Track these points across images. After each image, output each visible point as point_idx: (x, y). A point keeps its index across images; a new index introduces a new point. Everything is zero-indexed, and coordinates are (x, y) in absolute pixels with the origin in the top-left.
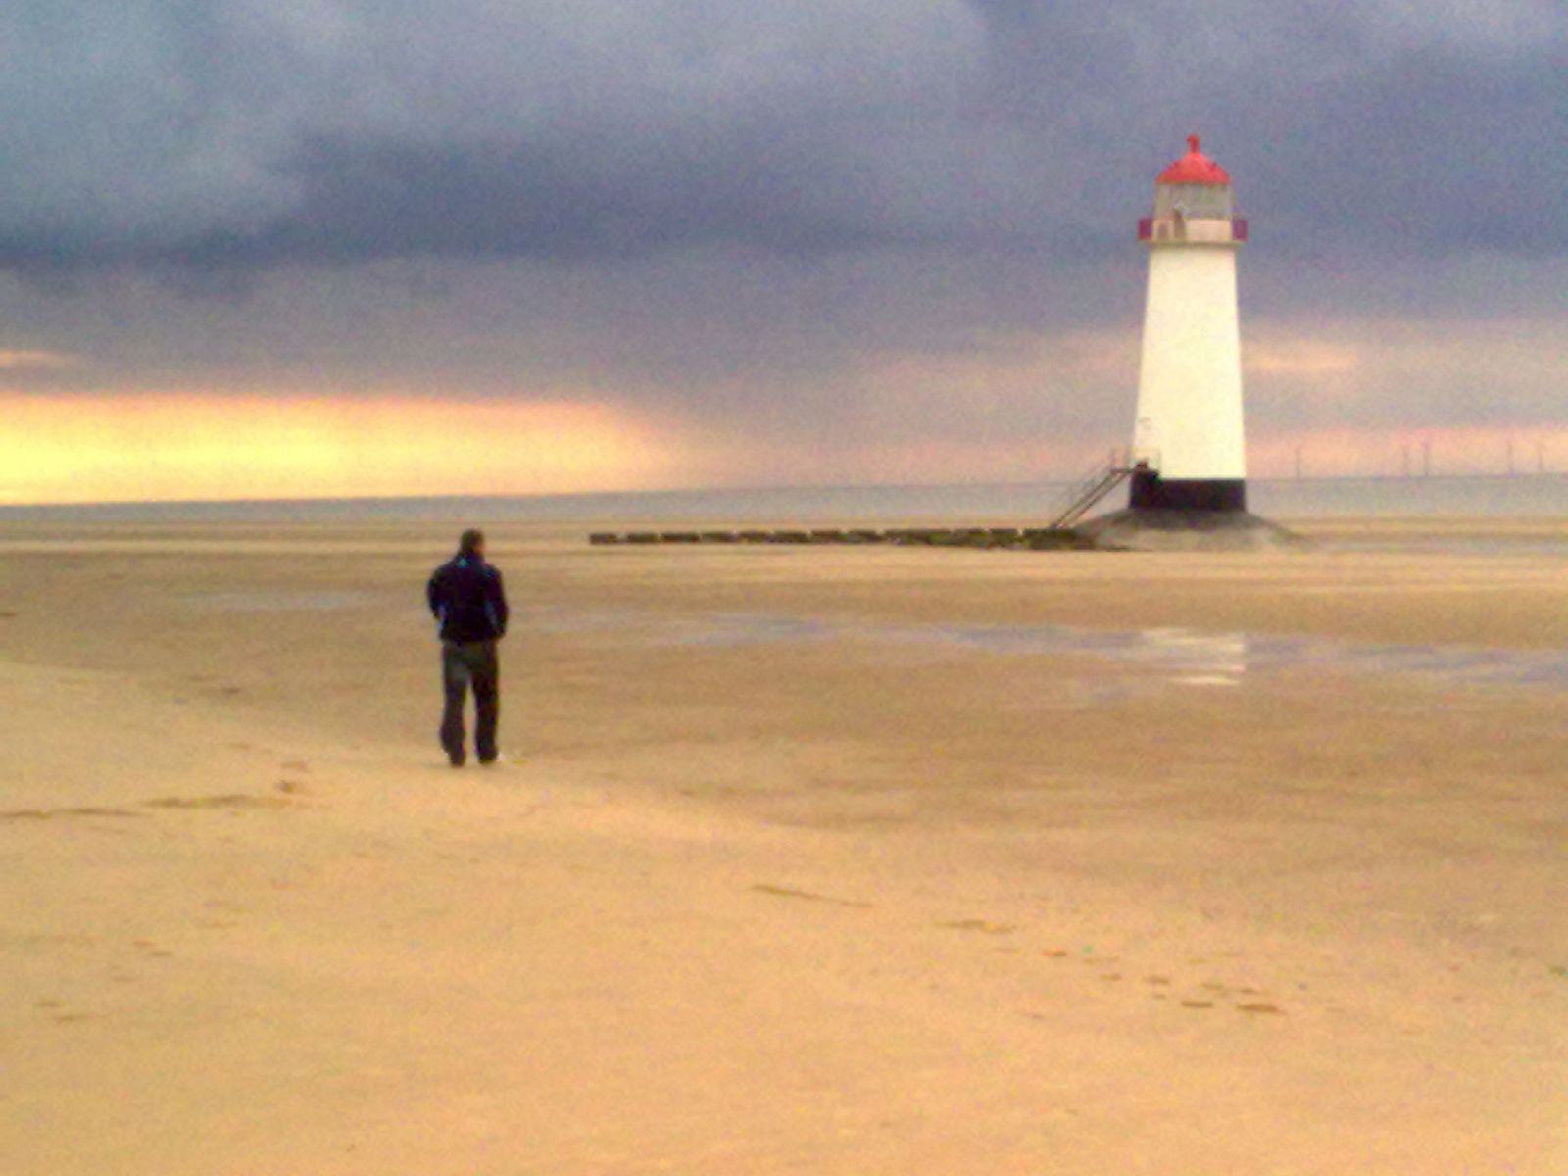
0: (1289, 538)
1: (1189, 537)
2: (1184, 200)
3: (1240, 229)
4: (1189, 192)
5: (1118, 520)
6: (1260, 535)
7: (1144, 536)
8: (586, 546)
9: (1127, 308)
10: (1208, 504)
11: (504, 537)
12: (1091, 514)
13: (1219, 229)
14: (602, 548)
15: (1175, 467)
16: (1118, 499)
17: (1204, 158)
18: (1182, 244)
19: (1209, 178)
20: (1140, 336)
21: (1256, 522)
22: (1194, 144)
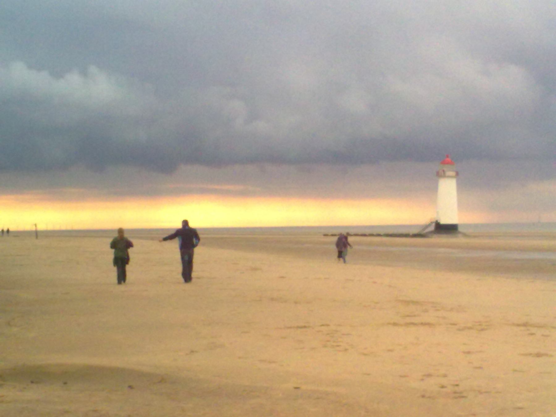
0: (465, 235)
1: (445, 235)
2: (446, 168)
3: (457, 174)
4: (446, 166)
5: (431, 232)
6: (460, 235)
7: (435, 236)
8: (323, 236)
9: (435, 189)
10: (451, 229)
11: (203, 234)
12: (425, 232)
13: (452, 173)
14: (326, 237)
15: (444, 221)
16: (432, 228)
17: (449, 159)
18: (444, 176)
19: (451, 163)
20: (437, 191)
21: (460, 233)
22: (447, 156)
